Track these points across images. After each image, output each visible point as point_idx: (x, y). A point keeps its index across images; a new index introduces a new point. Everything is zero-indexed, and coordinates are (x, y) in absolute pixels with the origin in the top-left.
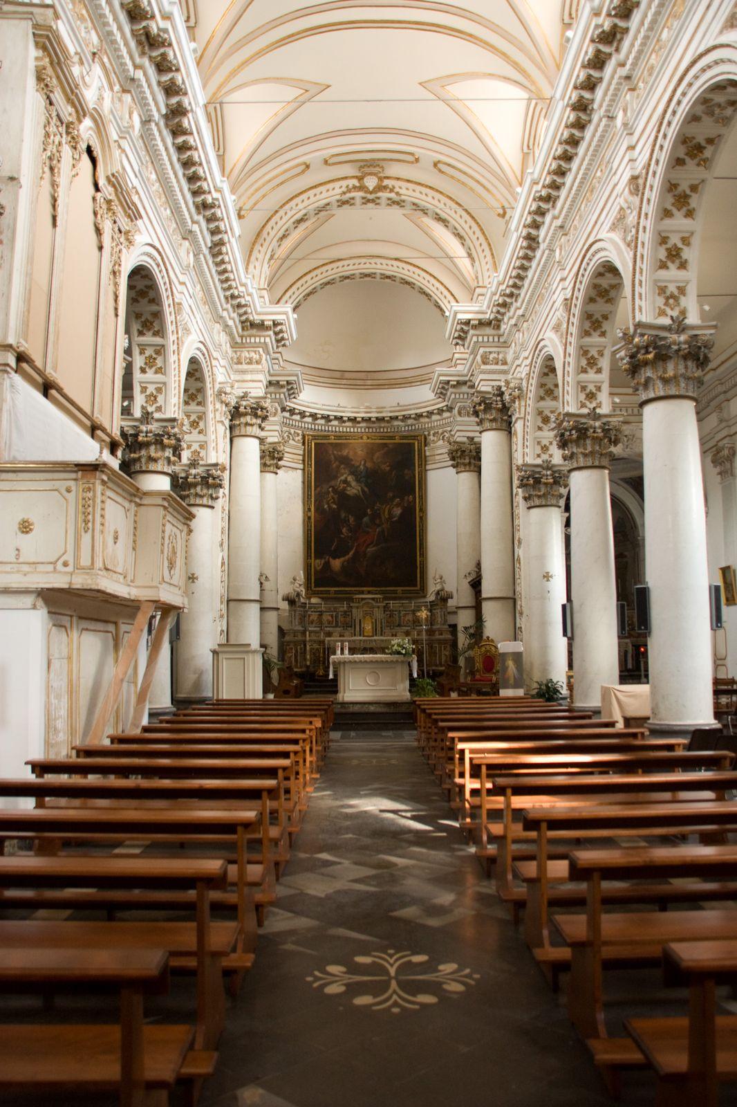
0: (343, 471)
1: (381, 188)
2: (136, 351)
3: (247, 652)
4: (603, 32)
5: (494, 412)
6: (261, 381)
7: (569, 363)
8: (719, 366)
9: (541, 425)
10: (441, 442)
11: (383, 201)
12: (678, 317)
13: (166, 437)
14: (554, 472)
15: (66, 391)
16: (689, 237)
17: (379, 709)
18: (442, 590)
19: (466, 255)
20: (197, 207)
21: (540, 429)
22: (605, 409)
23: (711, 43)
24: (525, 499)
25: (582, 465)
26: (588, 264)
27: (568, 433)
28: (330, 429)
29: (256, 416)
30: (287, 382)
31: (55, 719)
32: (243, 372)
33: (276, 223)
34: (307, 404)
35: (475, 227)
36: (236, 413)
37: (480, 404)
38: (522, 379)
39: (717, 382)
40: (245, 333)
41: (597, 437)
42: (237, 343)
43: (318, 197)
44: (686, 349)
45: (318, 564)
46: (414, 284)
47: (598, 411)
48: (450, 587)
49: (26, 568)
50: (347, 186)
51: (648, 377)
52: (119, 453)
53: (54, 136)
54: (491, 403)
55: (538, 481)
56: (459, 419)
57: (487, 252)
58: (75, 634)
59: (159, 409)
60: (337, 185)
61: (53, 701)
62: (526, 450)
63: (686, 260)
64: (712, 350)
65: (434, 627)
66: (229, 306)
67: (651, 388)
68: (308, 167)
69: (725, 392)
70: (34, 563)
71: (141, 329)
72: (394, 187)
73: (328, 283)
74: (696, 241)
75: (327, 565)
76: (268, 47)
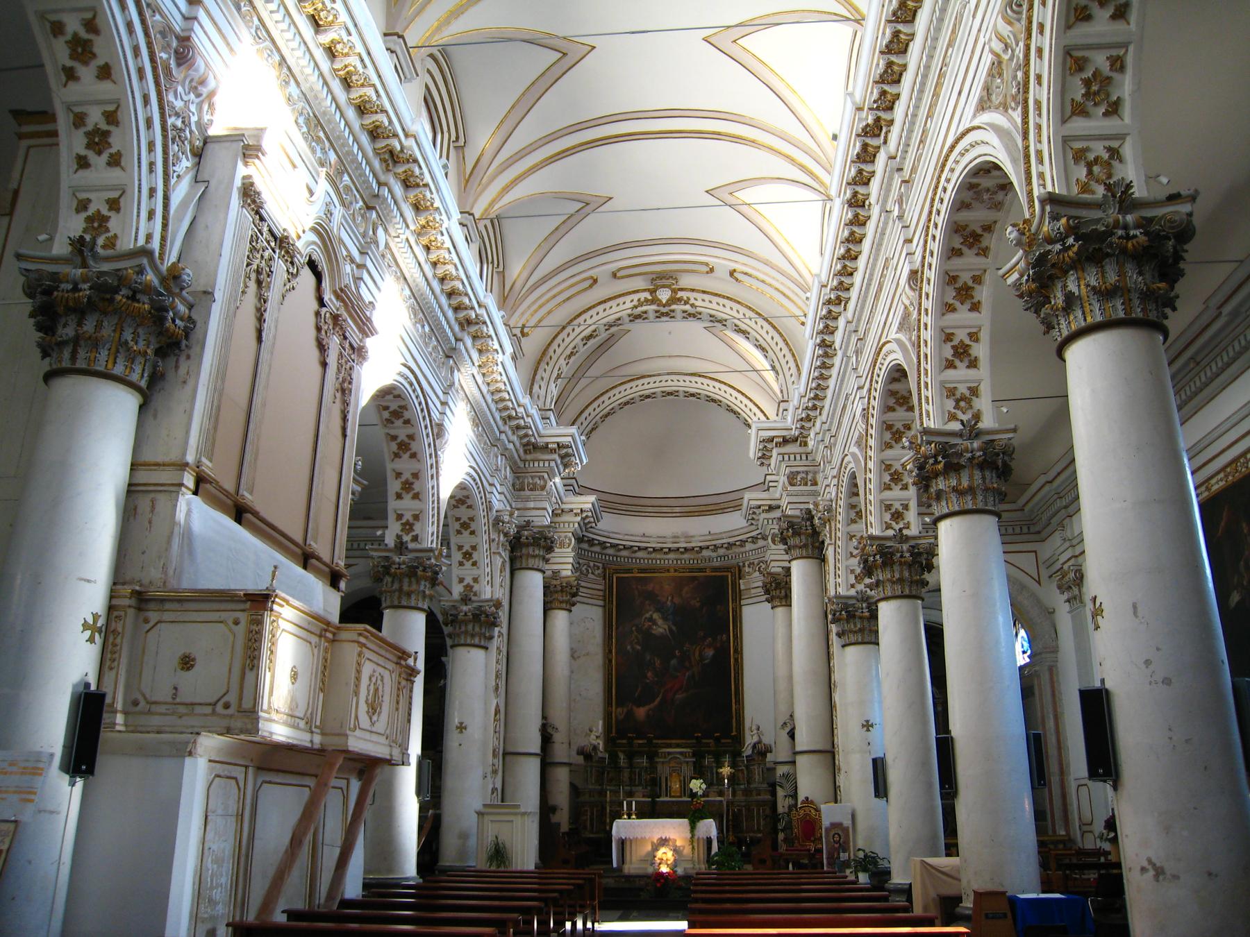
1: (674, 300)
3: (516, 814)
4: (867, 125)
8: (1056, 477)
11: (679, 315)
12: (969, 421)
13: (421, 568)
15: (263, 513)
18: (759, 742)
19: (769, 368)
20: (461, 325)
23: (968, 126)
24: (839, 635)
27: (871, 559)
31: (212, 888)
34: (606, 534)
39: (1056, 496)
40: (529, 457)
41: (905, 562)
42: (519, 467)
44: (980, 456)
46: (721, 402)
47: (905, 532)
49: (182, 709)
50: (639, 300)
52: (343, 585)
53: (264, 251)
60: (628, 299)
61: (210, 866)
62: (839, 580)
64: (1013, 456)
65: (752, 786)
68: (595, 281)
69: (1066, 507)
70: (192, 704)
72: (689, 299)
75: (630, 714)
76: (542, 162)
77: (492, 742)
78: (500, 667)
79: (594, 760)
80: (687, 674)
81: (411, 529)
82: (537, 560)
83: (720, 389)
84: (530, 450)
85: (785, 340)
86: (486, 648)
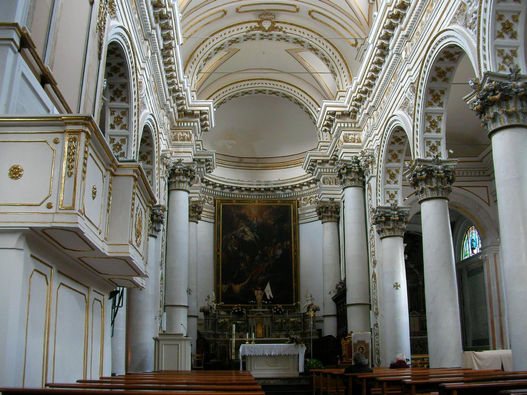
0: (241, 224)
1: (272, 28)
2: (108, 113)
3: (180, 340)
5: (353, 174)
6: (191, 152)
7: (417, 125)
9: (389, 180)
10: (309, 205)
14: (400, 212)
15: (59, 87)
16: (517, 16)
17: (280, 383)
18: (312, 305)
21: (388, 182)
22: (400, 204)
24: (379, 232)
25: (430, 196)
26: (432, 52)
28: (233, 196)
29: (186, 176)
30: (206, 159)
32: (179, 146)
33: (203, 49)
35: (336, 53)
36: (173, 174)
37: (343, 169)
38: (373, 150)
40: (181, 120)
41: (440, 176)
42: (174, 126)
43: (232, 33)
44: (522, 91)
45: (223, 288)
47: (440, 158)
48: (317, 303)
50: (251, 27)
51: (496, 113)
54: (352, 168)
55: (388, 219)
56: (324, 186)
57: (345, 69)
58: (55, 285)
59: (123, 155)
60: (244, 26)
63: (516, 32)
65: (306, 331)
66: (171, 97)
67: (498, 120)
68: (225, 13)
71: (112, 96)
72: (282, 28)
73: (234, 96)
74: (521, 18)
75: (230, 289)
77: (160, 297)
78: (163, 250)
79: (210, 315)
80: (265, 265)
81: (120, 149)
82: (185, 184)
83: (291, 90)
84: (182, 115)
85: (341, 55)
86: (156, 237)
